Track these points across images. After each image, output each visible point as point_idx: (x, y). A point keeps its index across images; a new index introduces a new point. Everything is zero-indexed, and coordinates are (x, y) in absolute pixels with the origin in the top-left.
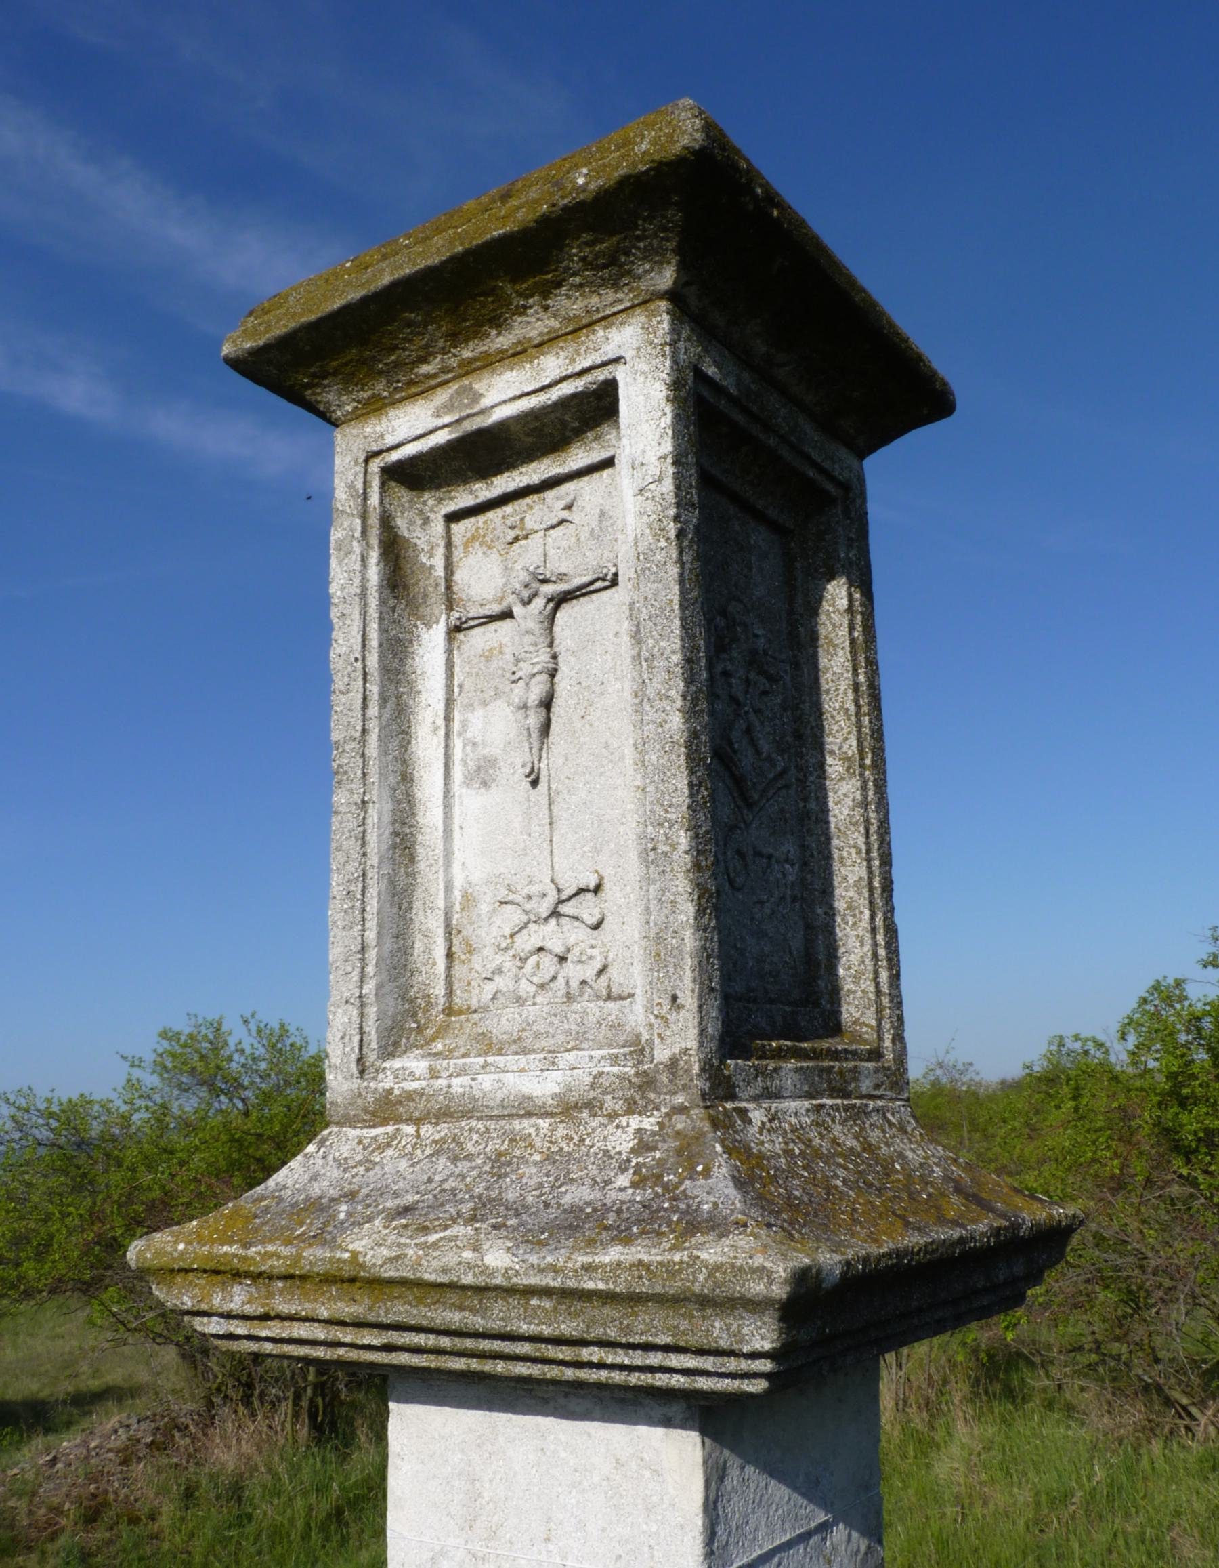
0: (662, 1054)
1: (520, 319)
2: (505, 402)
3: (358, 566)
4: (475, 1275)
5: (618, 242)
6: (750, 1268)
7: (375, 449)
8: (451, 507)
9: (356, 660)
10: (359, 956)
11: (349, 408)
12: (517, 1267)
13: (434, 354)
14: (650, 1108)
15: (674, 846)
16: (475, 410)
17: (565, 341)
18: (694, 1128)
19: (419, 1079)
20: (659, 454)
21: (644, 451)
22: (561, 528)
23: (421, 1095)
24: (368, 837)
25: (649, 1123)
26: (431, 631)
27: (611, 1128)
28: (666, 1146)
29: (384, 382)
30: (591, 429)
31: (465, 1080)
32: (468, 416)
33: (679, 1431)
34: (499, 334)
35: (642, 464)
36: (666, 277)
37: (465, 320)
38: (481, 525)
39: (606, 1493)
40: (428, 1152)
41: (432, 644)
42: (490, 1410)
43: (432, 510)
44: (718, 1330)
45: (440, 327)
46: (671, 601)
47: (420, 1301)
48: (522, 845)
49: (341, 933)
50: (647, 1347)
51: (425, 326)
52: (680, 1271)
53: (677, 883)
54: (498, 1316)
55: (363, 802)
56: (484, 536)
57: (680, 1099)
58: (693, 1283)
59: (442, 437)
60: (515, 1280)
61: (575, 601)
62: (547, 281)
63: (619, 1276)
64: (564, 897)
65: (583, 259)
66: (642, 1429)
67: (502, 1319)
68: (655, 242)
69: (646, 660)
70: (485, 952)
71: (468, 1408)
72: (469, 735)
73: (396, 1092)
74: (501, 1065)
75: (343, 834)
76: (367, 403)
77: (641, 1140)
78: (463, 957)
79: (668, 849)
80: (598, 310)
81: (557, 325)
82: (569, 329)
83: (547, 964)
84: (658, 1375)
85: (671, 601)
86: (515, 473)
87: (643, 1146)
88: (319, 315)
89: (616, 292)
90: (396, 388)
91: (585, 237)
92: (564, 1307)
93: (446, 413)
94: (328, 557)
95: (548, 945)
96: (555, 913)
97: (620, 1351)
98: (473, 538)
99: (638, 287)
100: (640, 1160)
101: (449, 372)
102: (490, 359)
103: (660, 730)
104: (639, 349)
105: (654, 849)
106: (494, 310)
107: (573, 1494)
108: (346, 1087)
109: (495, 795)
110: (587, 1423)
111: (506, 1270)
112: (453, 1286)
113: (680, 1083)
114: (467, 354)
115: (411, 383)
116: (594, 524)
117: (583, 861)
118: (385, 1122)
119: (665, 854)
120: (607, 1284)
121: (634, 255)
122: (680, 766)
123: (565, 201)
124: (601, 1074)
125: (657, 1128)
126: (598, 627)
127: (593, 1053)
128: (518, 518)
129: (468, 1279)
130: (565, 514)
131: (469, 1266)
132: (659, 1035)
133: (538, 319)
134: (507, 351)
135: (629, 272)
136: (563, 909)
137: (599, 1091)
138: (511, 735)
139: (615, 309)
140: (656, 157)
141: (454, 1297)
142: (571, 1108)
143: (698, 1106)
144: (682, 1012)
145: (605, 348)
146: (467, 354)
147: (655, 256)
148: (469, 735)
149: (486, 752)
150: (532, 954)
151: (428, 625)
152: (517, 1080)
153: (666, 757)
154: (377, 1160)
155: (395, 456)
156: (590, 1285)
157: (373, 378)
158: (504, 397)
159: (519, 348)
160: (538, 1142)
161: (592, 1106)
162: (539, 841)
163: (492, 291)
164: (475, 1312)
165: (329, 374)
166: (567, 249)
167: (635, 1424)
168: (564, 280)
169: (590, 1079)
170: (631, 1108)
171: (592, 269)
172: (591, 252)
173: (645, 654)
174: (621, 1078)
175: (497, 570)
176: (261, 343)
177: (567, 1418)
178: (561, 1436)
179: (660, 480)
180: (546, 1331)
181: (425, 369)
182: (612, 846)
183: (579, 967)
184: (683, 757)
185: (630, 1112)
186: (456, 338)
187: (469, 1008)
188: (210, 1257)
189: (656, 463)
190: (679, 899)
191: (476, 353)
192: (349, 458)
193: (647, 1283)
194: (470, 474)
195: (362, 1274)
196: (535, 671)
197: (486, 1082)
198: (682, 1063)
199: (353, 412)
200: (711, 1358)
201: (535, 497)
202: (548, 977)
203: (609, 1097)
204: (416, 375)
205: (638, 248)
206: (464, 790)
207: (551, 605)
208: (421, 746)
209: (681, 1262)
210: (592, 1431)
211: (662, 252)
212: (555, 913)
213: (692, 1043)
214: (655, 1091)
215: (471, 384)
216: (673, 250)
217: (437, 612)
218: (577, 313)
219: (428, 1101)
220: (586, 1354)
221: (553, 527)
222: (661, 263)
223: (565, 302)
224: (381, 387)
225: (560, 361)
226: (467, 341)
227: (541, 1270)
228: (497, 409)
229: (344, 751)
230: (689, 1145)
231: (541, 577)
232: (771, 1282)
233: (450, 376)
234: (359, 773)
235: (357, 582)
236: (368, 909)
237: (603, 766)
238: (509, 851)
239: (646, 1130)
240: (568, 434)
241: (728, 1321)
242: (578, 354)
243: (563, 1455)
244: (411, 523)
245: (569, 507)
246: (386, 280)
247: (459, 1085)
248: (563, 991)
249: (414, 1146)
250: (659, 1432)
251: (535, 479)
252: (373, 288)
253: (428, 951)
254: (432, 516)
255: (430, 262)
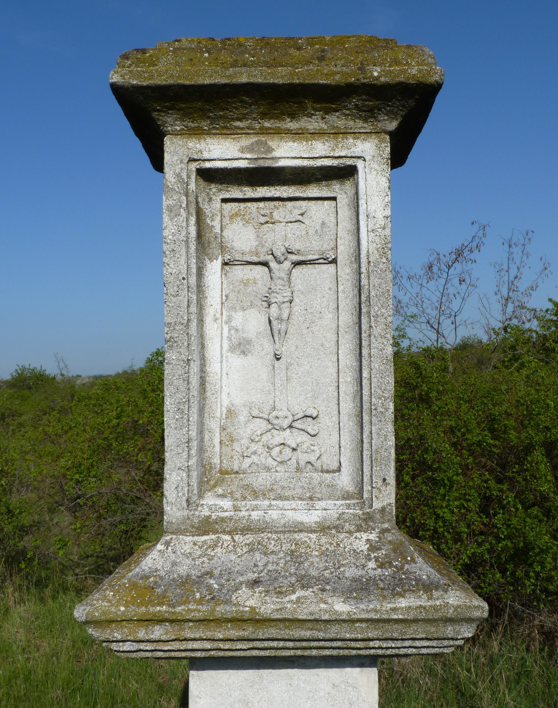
0: (377, 505)
1: (306, 119)
2: (288, 158)
3: (184, 224)
4: (330, 615)
5: (378, 104)
6: (474, 606)
7: (196, 157)
8: (227, 196)
9: (184, 279)
10: (187, 445)
11: (178, 128)
12: (355, 611)
13: (247, 119)
14: (370, 529)
15: (387, 409)
16: (268, 157)
17: (329, 137)
18: (397, 539)
19: (226, 511)
20: (384, 215)
21: (375, 211)
22: (296, 223)
23: (231, 520)
24: (191, 380)
25: (373, 536)
26: (212, 263)
27: (352, 539)
28: (386, 548)
29: (209, 122)
30: (326, 181)
31: (261, 513)
32: (263, 158)
33: (368, 668)
34: (291, 121)
35: (374, 217)
36: (393, 125)
37: (275, 110)
38: (242, 208)
39: (327, 700)
40: (245, 550)
41: (213, 271)
42: (258, 669)
43: (214, 194)
44: (449, 631)
45: (259, 108)
46: (389, 290)
47: (286, 627)
48: (268, 389)
49: (173, 432)
50: (414, 639)
51: (251, 105)
52: (440, 609)
53: (388, 427)
54: (333, 631)
55: (188, 360)
56: (244, 215)
57: (386, 526)
58: (447, 613)
59: (243, 164)
60: (354, 616)
61: (304, 266)
62: (332, 108)
63: (410, 612)
64: (295, 419)
65: (356, 105)
66: (348, 670)
67: (336, 633)
68: (395, 110)
69: (373, 317)
70: (243, 441)
71: (244, 669)
72: (233, 324)
73: (213, 517)
74: (281, 506)
75: (174, 376)
76: (193, 129)
77: (371, 545)
78: (227, 443)
79: (383, 410)
80: (351, 128)
81: (326, 127)
82: (332, 132)
83: (287, 452)
84: (401, 650)
85: (389, 290)
86: (272, 189)
87: (373, 548)
88: (193, 83)
89: (364, 123)
90: (214, 127)
91: (364, 97)
92: (373, 626)
93: (248, 152)
94: (162, 213)
95: (289, 442)
96: (291, 427)
97: (390, 642)
98: (236, 214)
99: (377, 125)
100: (375, 554)
101: (251, 129)
102: (280, 131)
103: (380, 352)
104: (374, 156)
105: (375, 409)
106: (295, 111)
107: (309, 702)
108: (179, 514)
109: (249, 360)
110: (317, 670)
111: (349, 612)
112: (316, 621)
113: (386, 519)
114: (267, 124)
115: (225, 128)
116: (318, 227)
117: (307, 401)
118: (206, 533)
119: (382, 413)
120: (404, 615)
121: (382, 111)
122: (391, 372)
123: (365, 81)
124: (343, 513)
125: (378, 539)
126: (318, 282)
127: (336, 502)
128: (268, 211)
129: (326, 617)
130: (300, 218)
131: (326, 611)
132: (376, 496)
133: (316, 122)
134: (292, 130)
135: (375, 117)
136: (296, 424)
137: (342, 521)
138: (261, 329)
139: (361, 131)
140: (421, 80)
141: (310, 625)
142: (326, 528)
143: (395, 529)
144: (388, 487)
145: (353, 149)
146: (267, 124)
147: (391, 115)
148: (233, 324)
149: (245, 335)
150: (276, 446)
151: (211, 260)
152: (294, 515)
153: (384, 366)
154: (213, 554)
155: (208, 165)
156: (395, 617)
157: (203, 119)
158: (288, 155)
159: (300, 131)
160: (312, 544)
161: (338, 528)
162: (281, 388)
163: (300, 103)
164: (319, 631)
165: (175, 108)
166: (351, 98)
167: (344, 667)
168: (341, 110)
169: (338, 515)
170: (359, 529)
171: (358, 110)
172: (362, 104)
173: (372, 313)
174: (354, 515)
175: (252, 236)
176: (145, 84)
177: (306, 668)
178: (301, 677)
179: (384, 228)
180: (360, 636)
181: (238, 124)
182: (324, 396)
183: (305, 455)
184: (392, 368)
185: (358, 531)
186: (265, 116)
187: (232, 470)
188: (147, 613)
189: (382, 219)
190: (388, 434)
191: (273, 126)
192: (175, 158)
193: (424, 615)
194: (244, 182)
195: (257, 617)
196: (285, 300)
197: (274, 514)
198: (388, 510)
199: (179, 131)
200: (436, 641)
201: (280, 203)
202: (287, 458)
203: (347, 524)
204: (231, 125)
205: (385, 109)
206: (229, 354)
207: (293, 266)
208: (208, 327)
209: (441, 605)
210: (320, 673)
211: (396, 114)
212: (291, 427)
213: (393, 501)
214: (372, 522)
215: (266, 140)
216: (402, 116)
217: (216, 253)
218: (339, 126)
219: (236, 523)
220: (371, 644)
221: (291, 222)
222: (393, 119)
223: (335, 119)
224: (205, 125)
225: (326, 147)
226: (271, 118)
227: (368, 612)
228: (282, 160)
229: (174, 329)
230: (398, 547)
231: (289, 251)
232: (483, 611)
233: (252, 131)
234: (186, 344)
235: (184, 233)
236: (191, 419)
237: (320, 355)
238: (259, 391)
239: (372, 540)
240: (312, 179)
241: (455, 627)
242: (337, 147)
243: (302, 685)
244: (204, 200)
245: (302, 215)
246: (244, 79)
247: (255, 515)
248: (295, 465)
249: (234, 546)
250: (357, 670)
251: (285, 195)
252: (234, 81)
253: (211, 439)
254: (214, 197)
255: (276, 81)
